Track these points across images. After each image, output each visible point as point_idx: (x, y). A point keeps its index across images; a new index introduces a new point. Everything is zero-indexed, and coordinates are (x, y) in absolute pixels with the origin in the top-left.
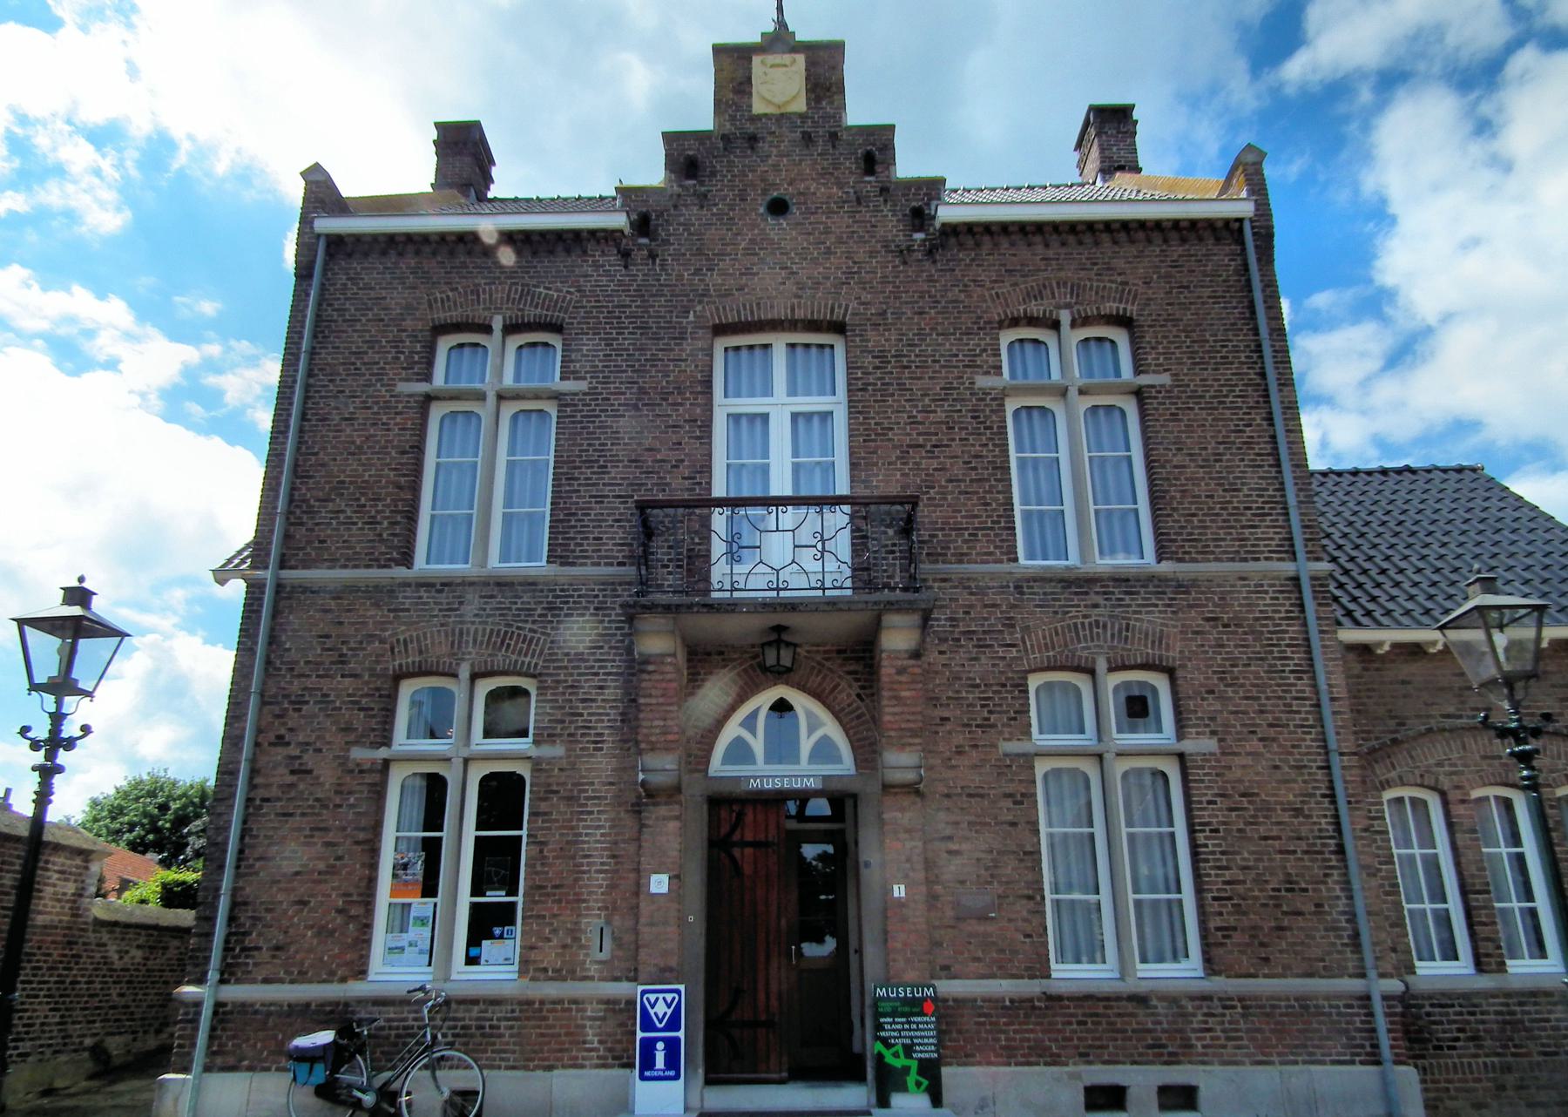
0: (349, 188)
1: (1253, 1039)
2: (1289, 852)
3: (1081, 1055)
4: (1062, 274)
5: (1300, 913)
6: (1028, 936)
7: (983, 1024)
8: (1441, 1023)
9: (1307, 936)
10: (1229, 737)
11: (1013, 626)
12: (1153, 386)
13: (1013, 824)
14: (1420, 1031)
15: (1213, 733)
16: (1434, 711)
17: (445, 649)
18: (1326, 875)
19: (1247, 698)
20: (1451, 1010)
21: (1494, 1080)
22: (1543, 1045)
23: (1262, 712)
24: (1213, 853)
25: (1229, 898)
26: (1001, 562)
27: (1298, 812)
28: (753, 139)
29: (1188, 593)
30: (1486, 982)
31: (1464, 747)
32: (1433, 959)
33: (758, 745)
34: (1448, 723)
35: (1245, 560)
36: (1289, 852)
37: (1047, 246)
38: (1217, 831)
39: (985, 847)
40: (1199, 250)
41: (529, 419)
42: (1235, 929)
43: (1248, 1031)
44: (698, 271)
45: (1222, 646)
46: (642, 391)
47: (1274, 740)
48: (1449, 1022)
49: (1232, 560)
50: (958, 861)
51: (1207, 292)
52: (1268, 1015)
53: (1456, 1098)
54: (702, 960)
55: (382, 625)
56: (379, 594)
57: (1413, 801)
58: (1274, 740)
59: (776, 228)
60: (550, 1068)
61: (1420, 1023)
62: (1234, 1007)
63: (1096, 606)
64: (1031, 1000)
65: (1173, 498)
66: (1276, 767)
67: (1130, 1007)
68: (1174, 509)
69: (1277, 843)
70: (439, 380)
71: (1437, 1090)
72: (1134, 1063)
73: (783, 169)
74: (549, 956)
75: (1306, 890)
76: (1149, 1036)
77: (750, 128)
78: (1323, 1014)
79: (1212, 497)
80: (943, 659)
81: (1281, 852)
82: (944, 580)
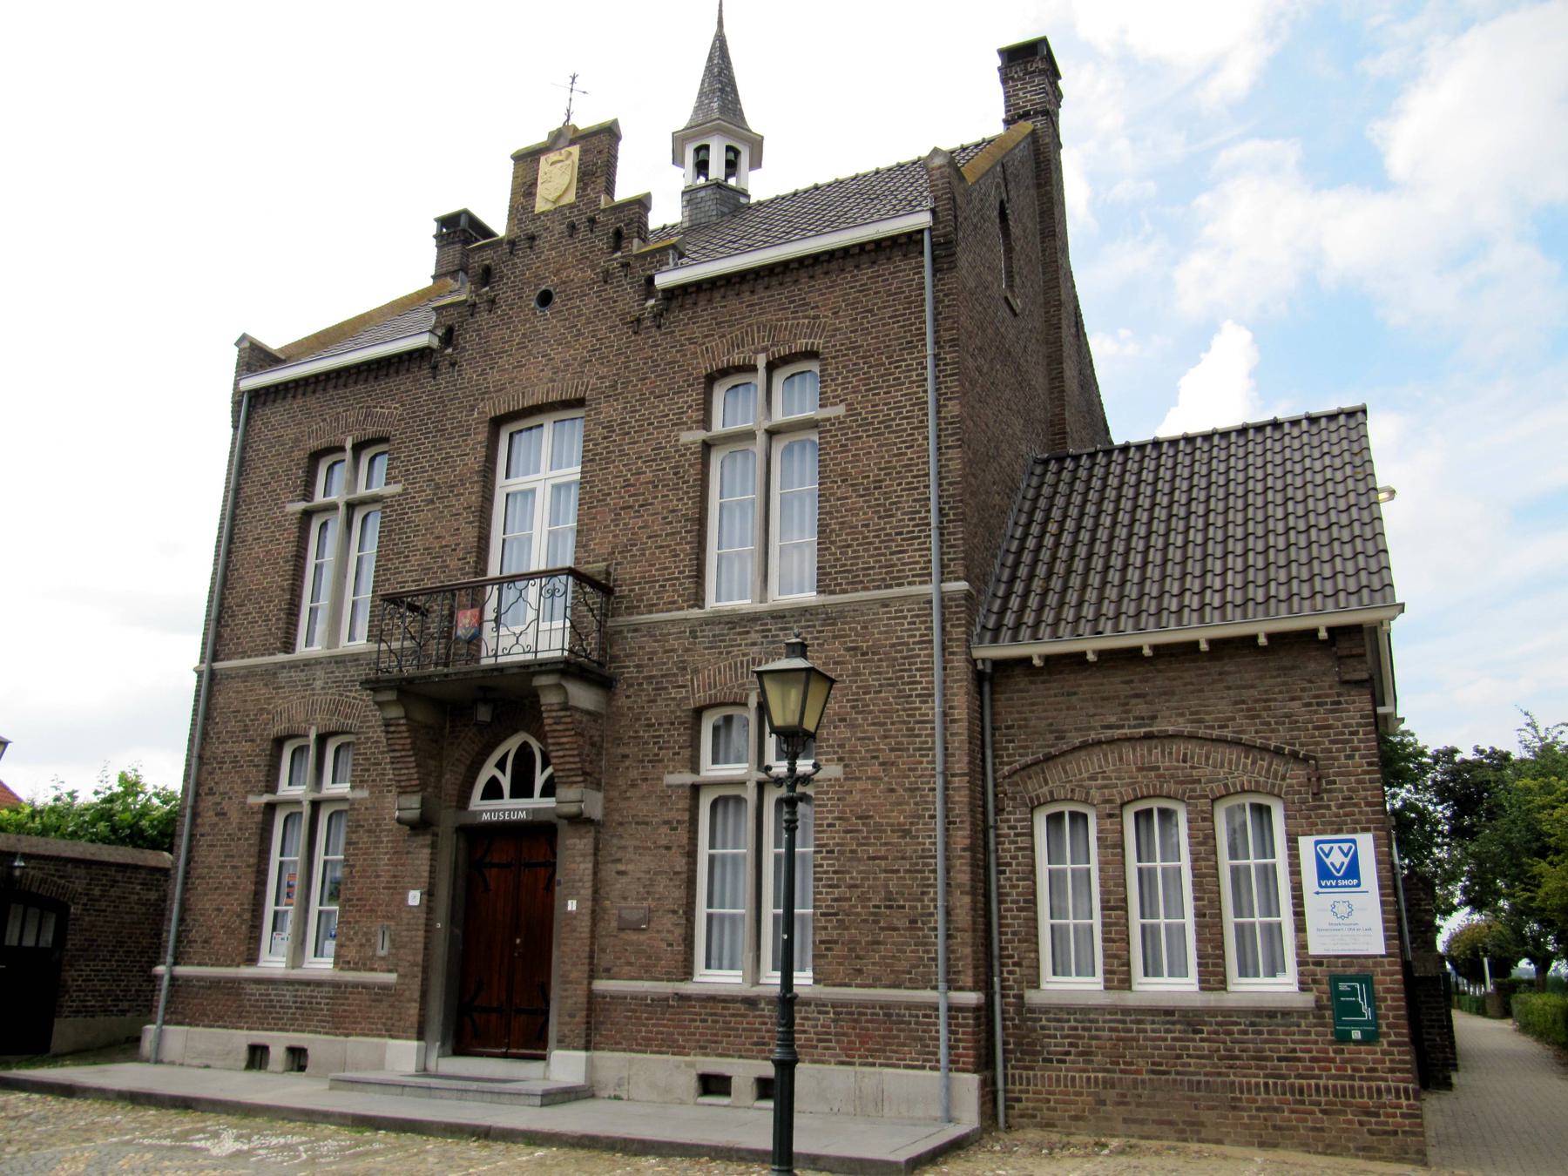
0: (274, 341)
1: (838, 1042)
2: (893, 872)
3: (702, 1048)
4: (763, 318)
5: (896, 929)
6: (670, 945)
7: (629, 1018)
8: (1055, 1037)
9: (899, 951)
10: (853, 763)
11: (685, 669)
12: (829, 419)
13: (668, 848)
14: (1033, 1044)
15: (840, 759)
16: (1096, 722)
17: (303, 716)
18: (923, 893)
19: (874, 724)
20: (1235, 1028)
21: (1096, 1094)
22: (1154, 1064)
23: (886, 737)
24: (826, 872)
25: (836, 914)
26: (681, 609)
27: (906, 833)
28: (532, 238)
29: (834, 624)
30: (1213, 999)
31: (1121, 759)
32: (1256, 975)
33: (506, 782)
34: (1109, 733)
35: (890, 586)
36: (893, 872)
37: (752, 292)
38: (832, 852)
39: (645, 867)
40: (885, 268)
41: (735, 460)
42: (836, 942)
43: (837, 1034)
44: (483, 373)
45: (858, 674)
46: (438, 487)
47: (893, 764)
48: (1063, 1037)
49: (879, 587)
50: (624, 880)
51: (889, 312)
52: (856, 1021)
53: (1055, 1110)
54: (555, 953)
55: (269, 700)
56: (271, 673)
57: (1073, 815)
58: (893, 764)
59: (548, 323)
60: (347, 1035)
61: (1034, 1035)
62: (827, 1013)
63: (754, 644)
64: (667, 999)
65: (832, 531)
66: (892, 790)
67: (742, 1008)
68: (832, 543)
69: (883, 863)
70: (718, 427)
71: (1038, 1100)
72: (740, 1057)
73: (553, 263)
74: (351, 953)
75: (903, 907)
76: (755, 1034)
77: (531, 228)
78: (903, 1022)
79: (867, 526)
80: (628, 702)
81: (886, 871)
82: (636, 630)
